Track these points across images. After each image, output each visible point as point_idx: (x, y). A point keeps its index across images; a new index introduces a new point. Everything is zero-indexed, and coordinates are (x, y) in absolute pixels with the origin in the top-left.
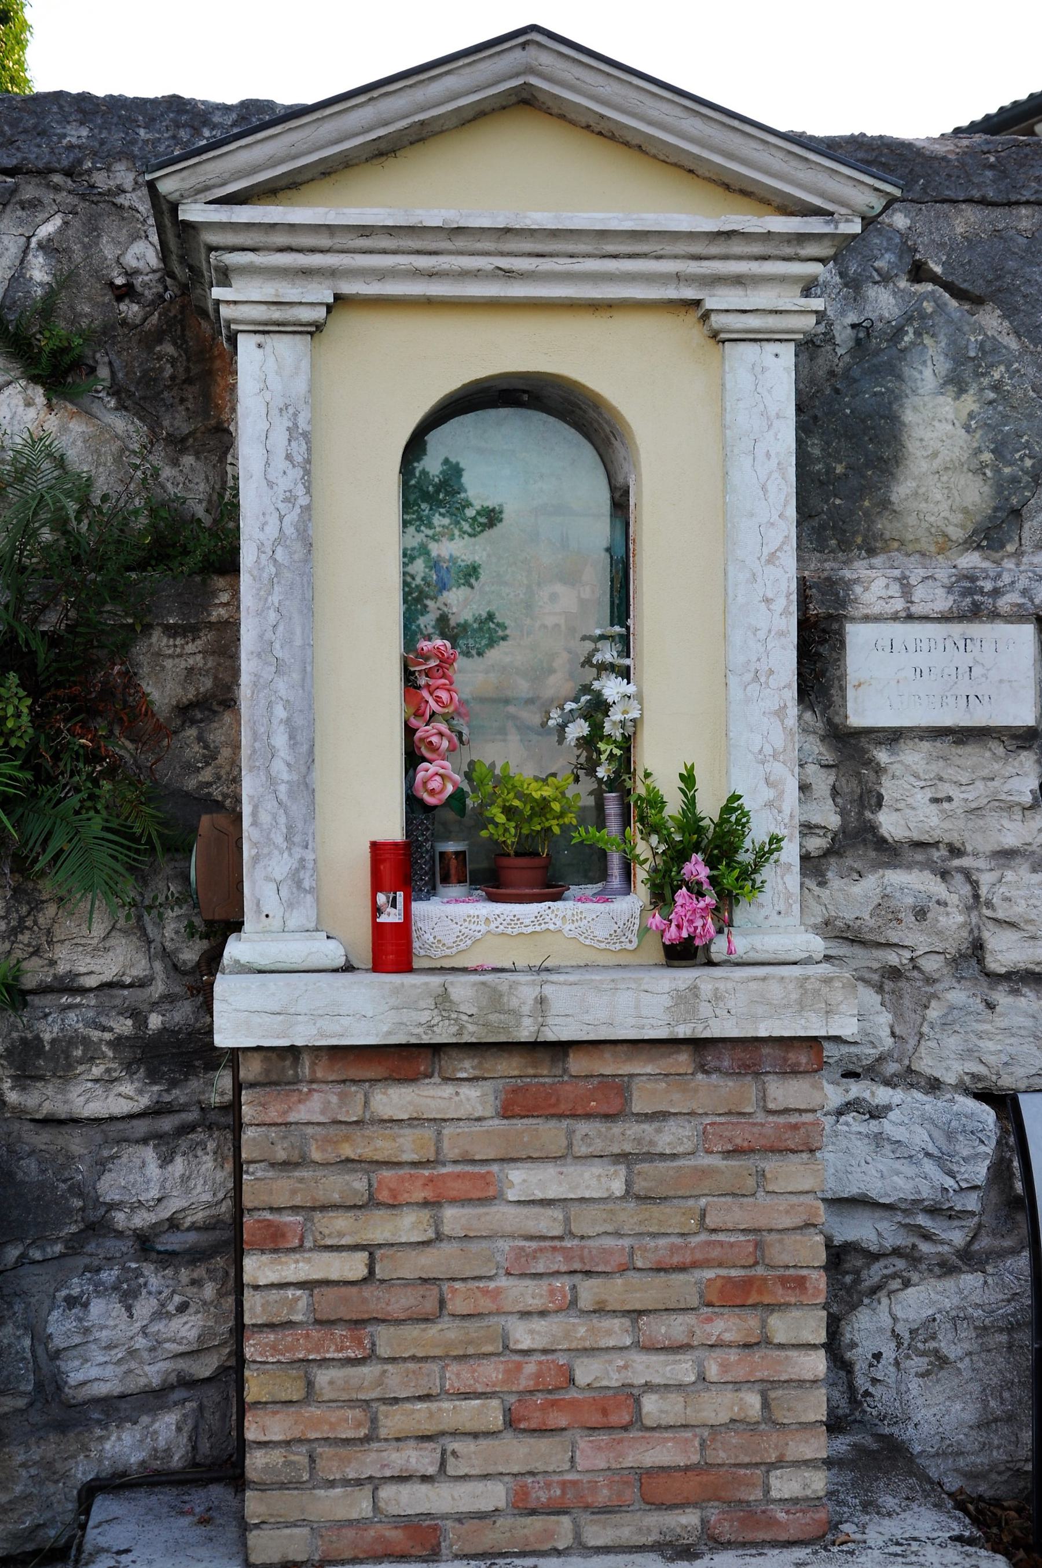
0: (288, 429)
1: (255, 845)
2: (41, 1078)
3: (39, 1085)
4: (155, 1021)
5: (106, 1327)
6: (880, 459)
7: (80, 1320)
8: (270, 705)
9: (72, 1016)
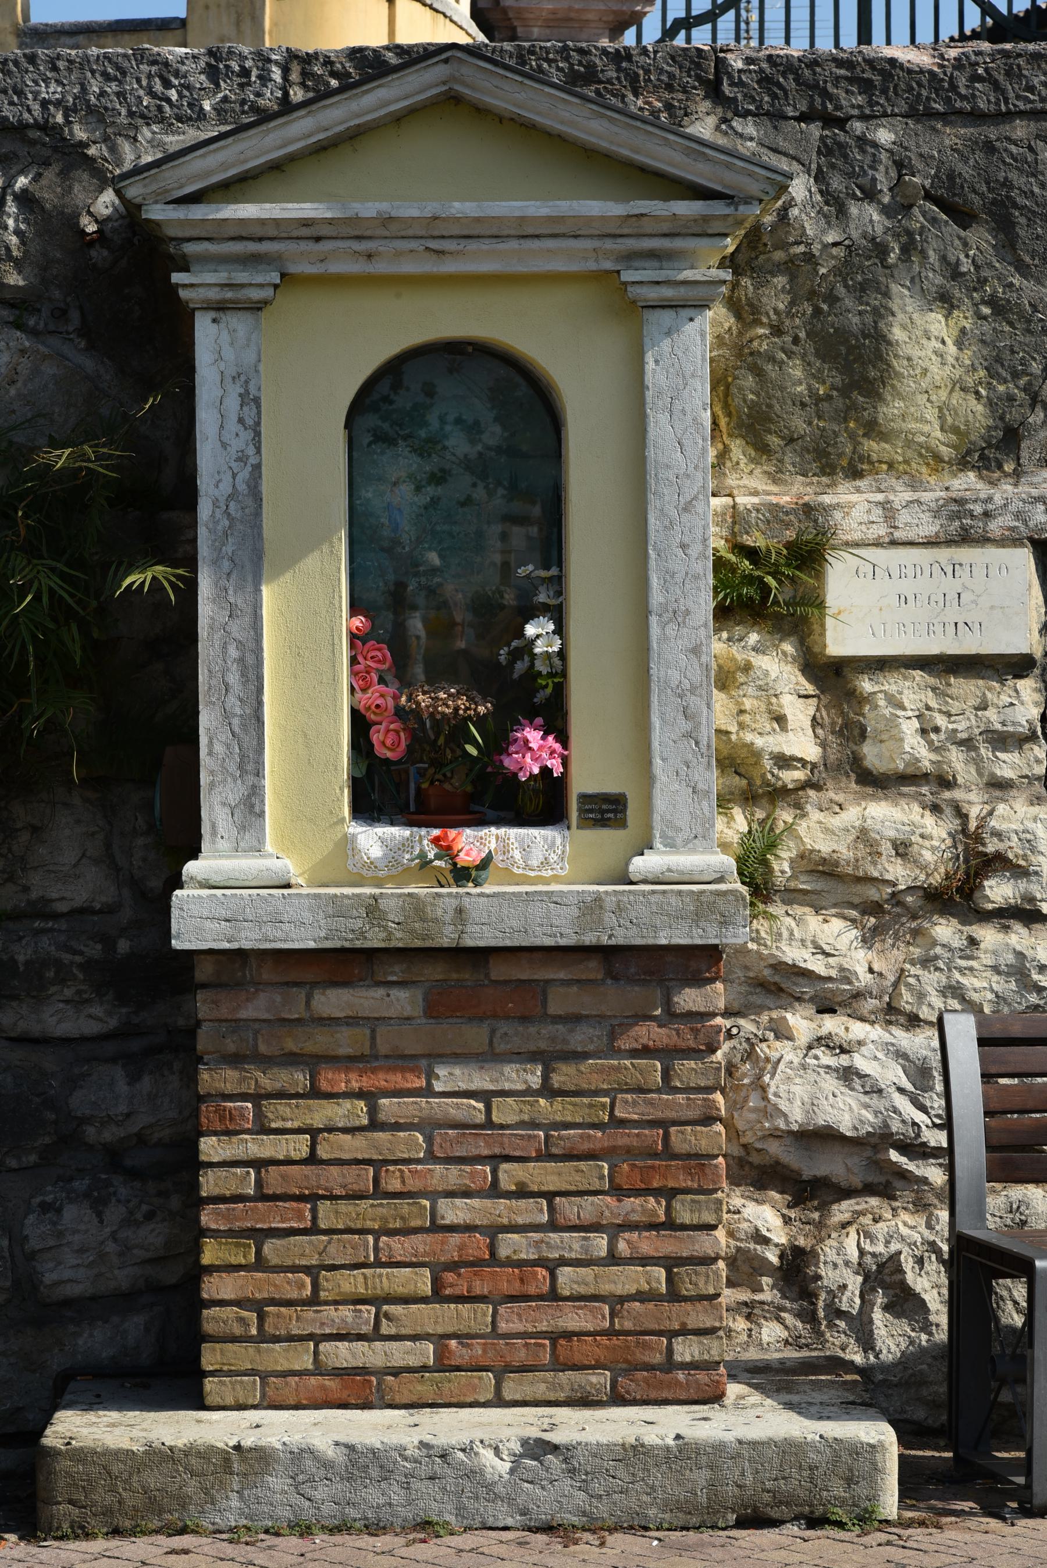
0: (240, 395)
1: (212, 773)
2: (15, 997)
3: (14, 1004)
4: (123, 946)
5: (78, 1231)
6: (866, 379)
7: (54, 1224)
8: (225, 647)
9: (45, 941)
